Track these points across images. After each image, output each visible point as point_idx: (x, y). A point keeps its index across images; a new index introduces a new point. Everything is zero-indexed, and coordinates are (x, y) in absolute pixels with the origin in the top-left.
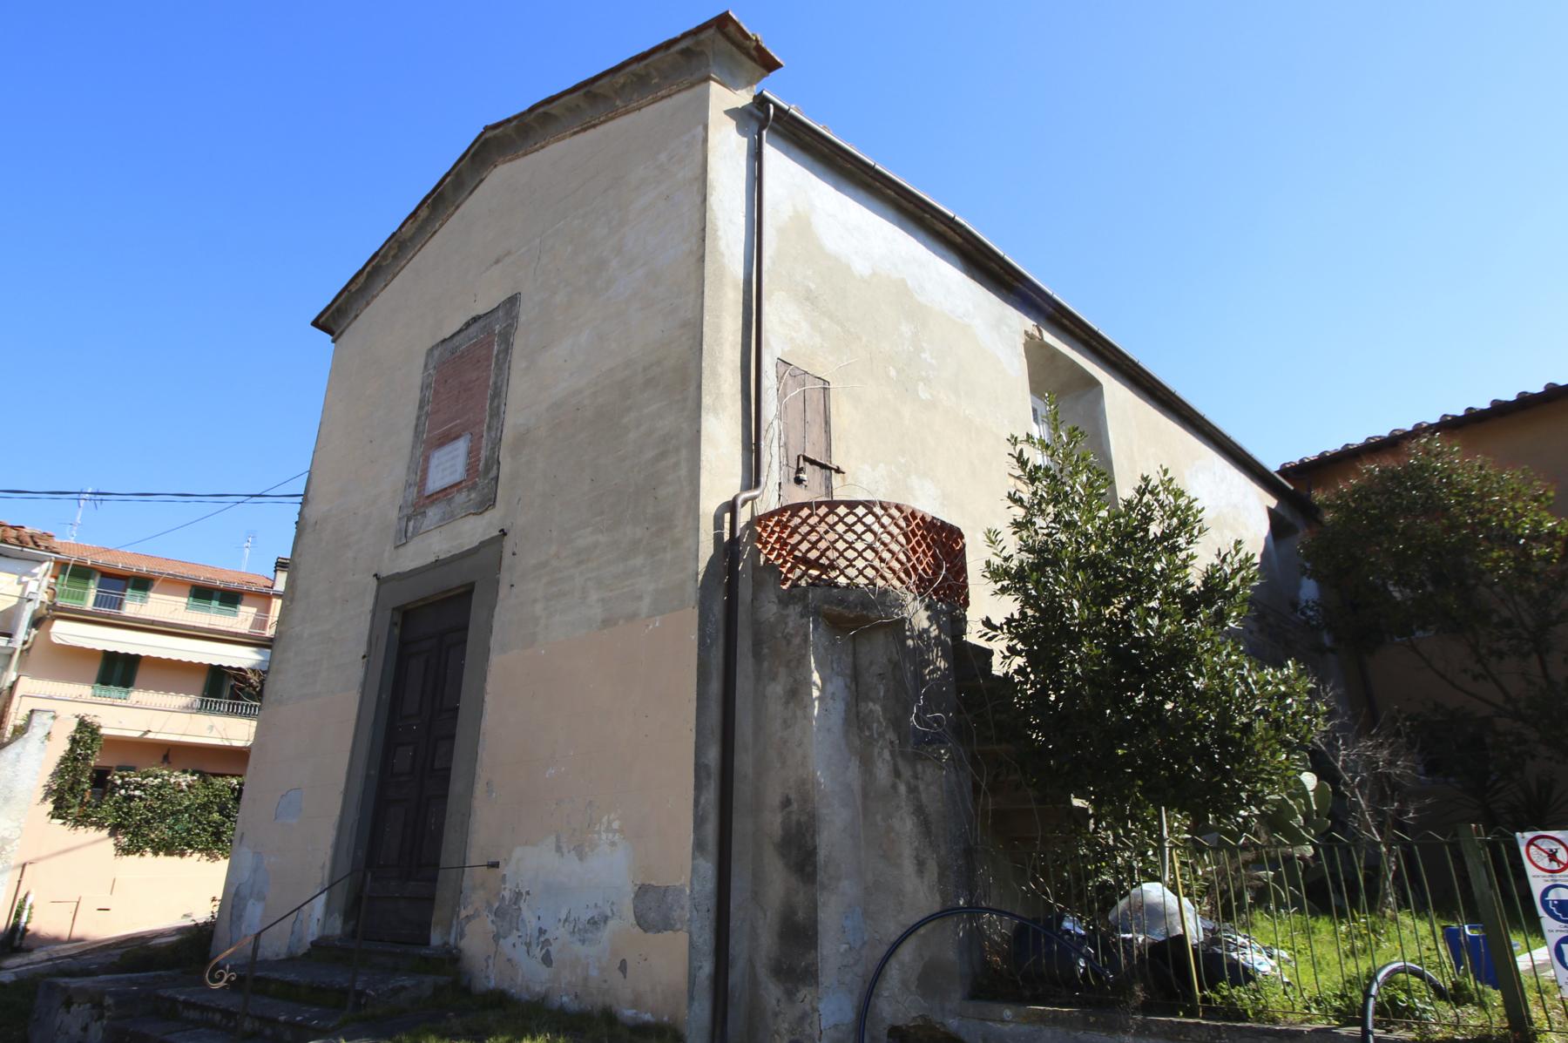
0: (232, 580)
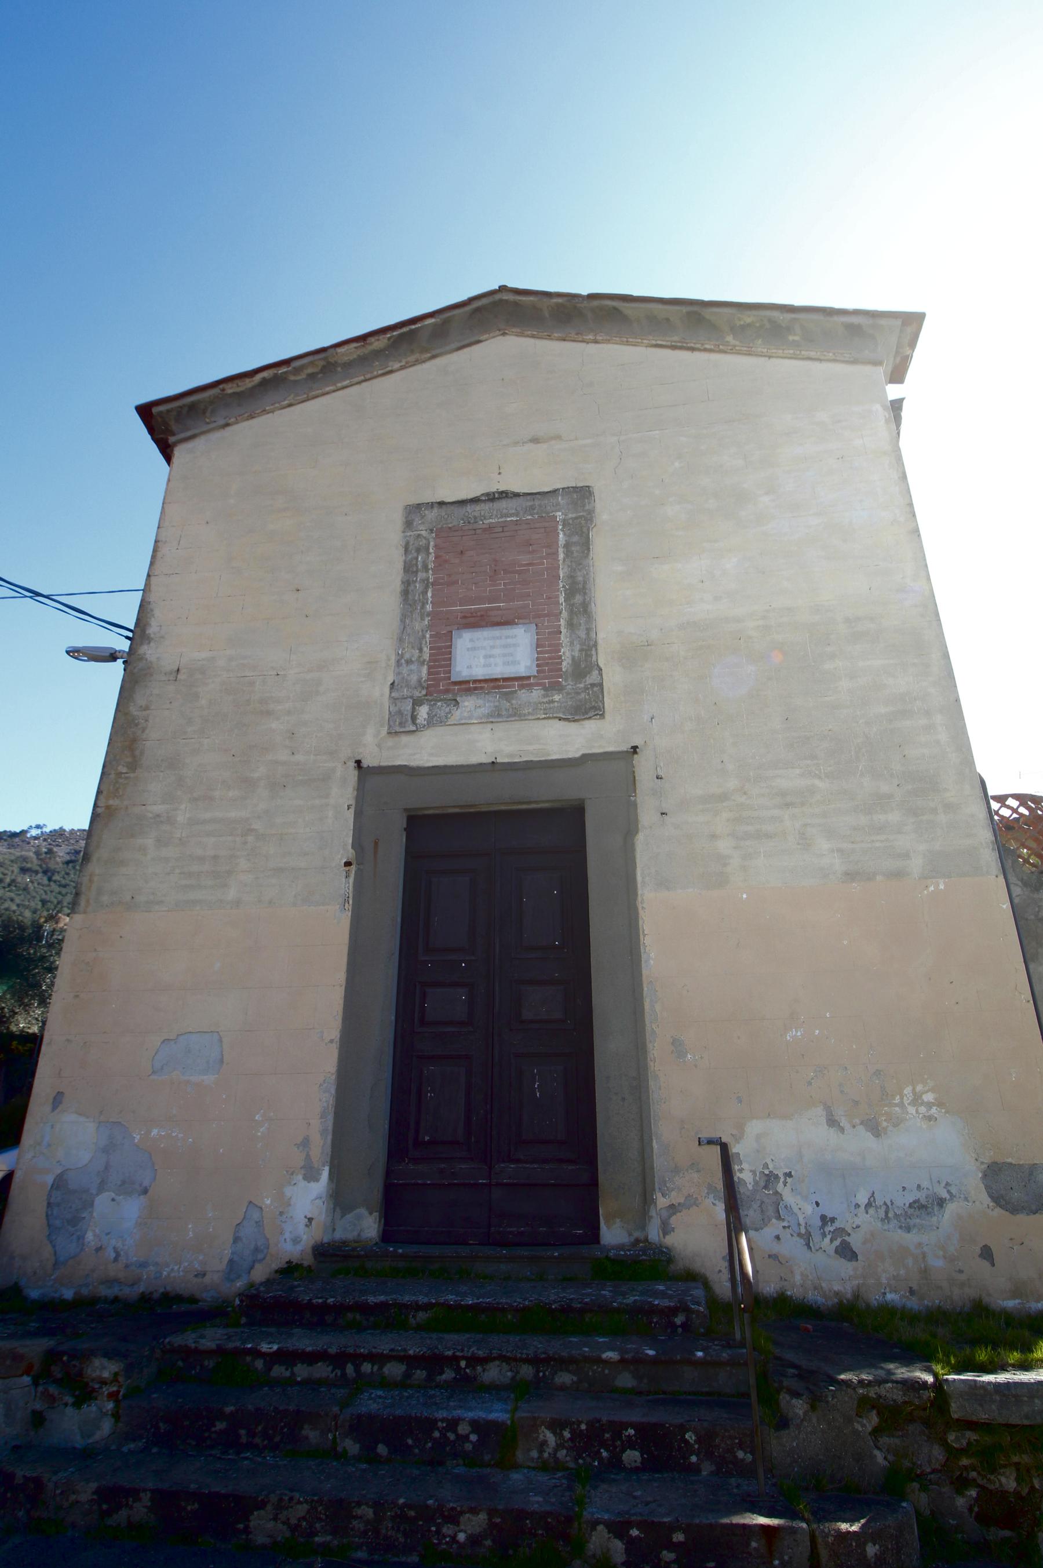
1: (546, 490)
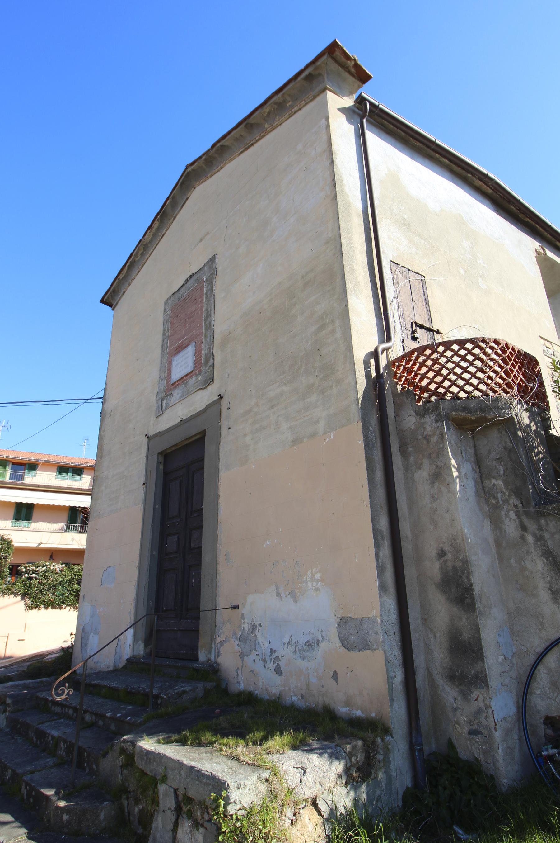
0: (77, 462)
1: (202, 266)
